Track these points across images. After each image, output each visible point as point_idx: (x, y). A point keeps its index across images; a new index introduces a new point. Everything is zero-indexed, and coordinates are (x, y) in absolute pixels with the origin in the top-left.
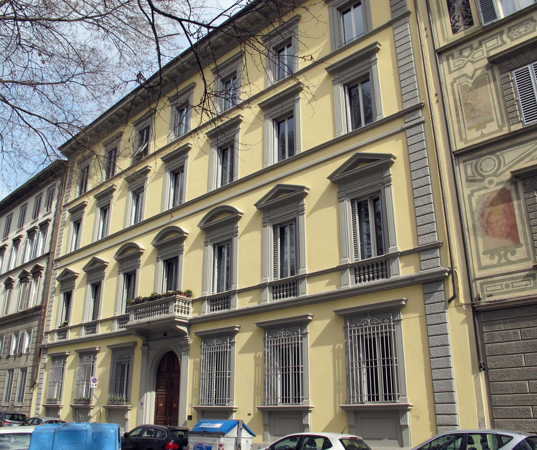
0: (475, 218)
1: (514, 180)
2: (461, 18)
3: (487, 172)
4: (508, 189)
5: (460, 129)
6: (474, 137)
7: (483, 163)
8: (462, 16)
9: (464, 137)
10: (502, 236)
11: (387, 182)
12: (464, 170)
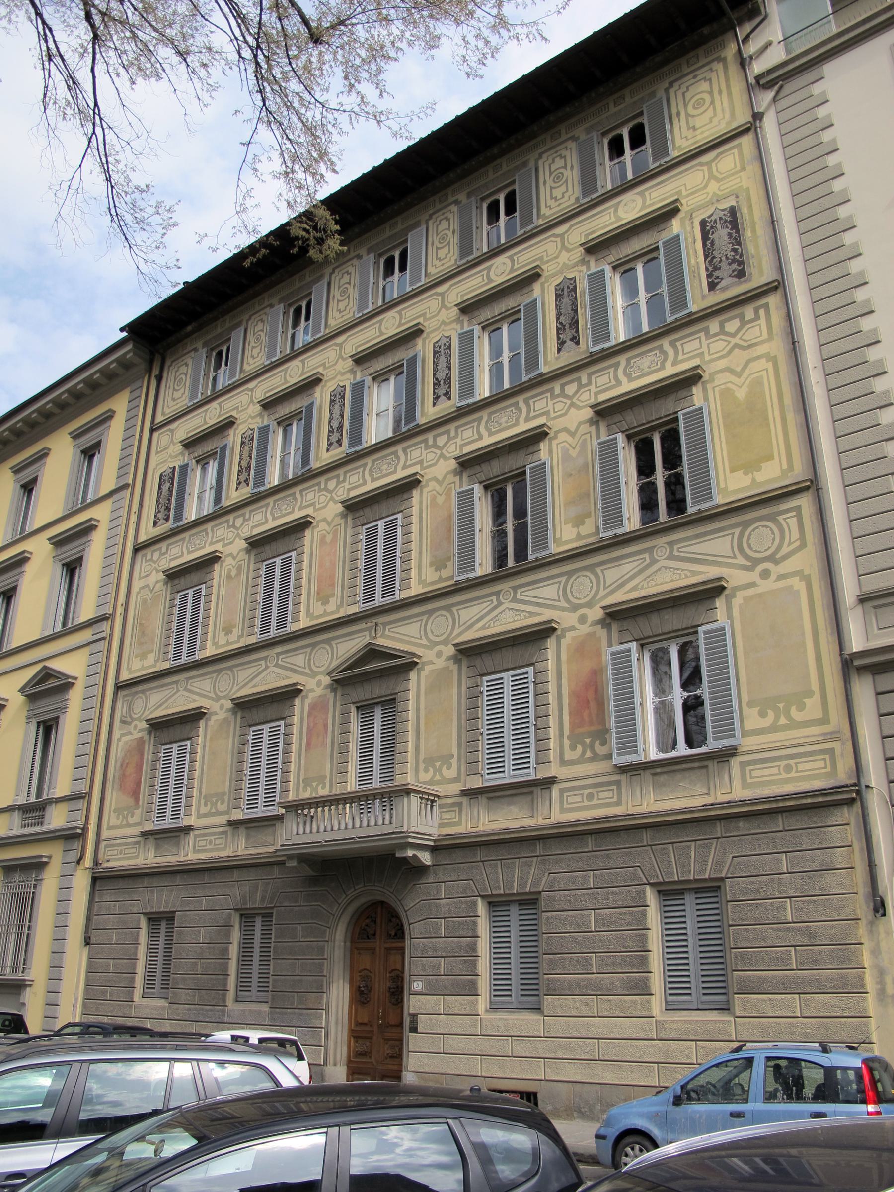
1: (608, 621)
4: (795, 588)
8: (727, 258)
11: (63, 709)
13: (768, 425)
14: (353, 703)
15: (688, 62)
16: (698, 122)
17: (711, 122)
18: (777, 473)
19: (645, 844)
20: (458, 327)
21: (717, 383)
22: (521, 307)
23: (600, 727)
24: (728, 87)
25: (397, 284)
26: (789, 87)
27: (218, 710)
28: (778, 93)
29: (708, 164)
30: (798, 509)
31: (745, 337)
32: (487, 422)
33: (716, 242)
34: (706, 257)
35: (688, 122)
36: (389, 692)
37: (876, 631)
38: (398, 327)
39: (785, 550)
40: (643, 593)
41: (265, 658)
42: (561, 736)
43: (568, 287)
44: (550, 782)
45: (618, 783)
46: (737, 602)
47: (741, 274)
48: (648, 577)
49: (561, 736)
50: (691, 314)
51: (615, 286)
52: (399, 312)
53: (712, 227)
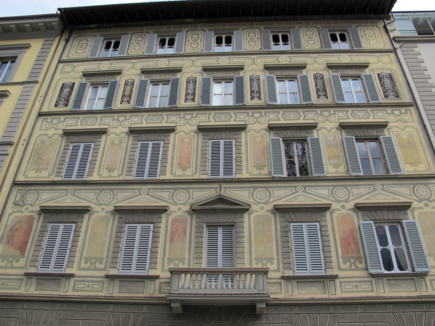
0: (6, 231)
1: (41, 212)
2: (63, 99)
3: (28, 201)
5: (26, 168)
6: (32, 176)
7: (29, 195)
9: (26, 174)
10: (16, 248)
12: (16, 195)
13: (418, 151)
14: (205, 223)
19: (110, 311)
20: (139, 77)
22: (110, 83)
23: (358, 255)
25: (111, 53)
27: (100, 211)
32: (146, 118)
36: (231, 221)
40: (372, 202)
41: (66, 190)
42: (337, 256)
43: (193, 80)
44: (334, 278)
45: (371, 282)
48: (374, 196)
49: (337, 256)
51: (89, 91)
52: (111, 64)
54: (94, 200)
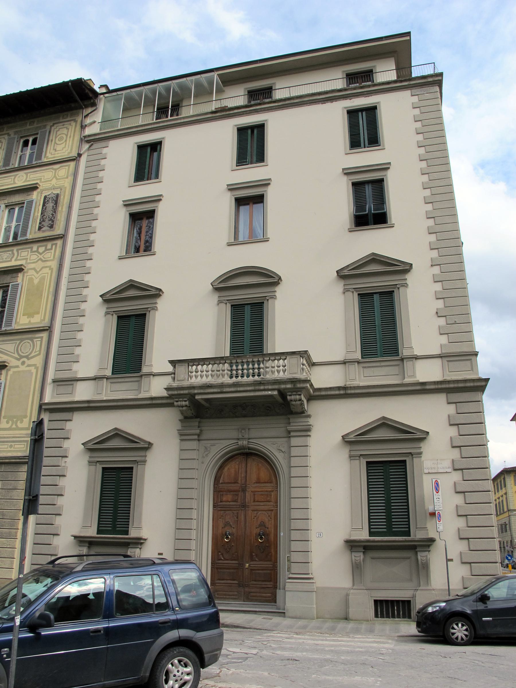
13: (42, 298)
15: (63, 116)
16: (58, 148)
17: (63, 150)
18: (39, 321)
21: (29, 274)
24: (74, 135)
26: (96, 145)
28: (90, 146)
29: (55, 170)
30: (42, 337)
31: (45, 256)
33: (47, 208)
34: (42, 214)
35: (54, 146)
37: (362, 377)
38: (24, 182)
39: (33, 354)
46: (10, 373)
47: (51, 227)
50: (27, 239)
53: (48, 201)
54: (14, 353)
